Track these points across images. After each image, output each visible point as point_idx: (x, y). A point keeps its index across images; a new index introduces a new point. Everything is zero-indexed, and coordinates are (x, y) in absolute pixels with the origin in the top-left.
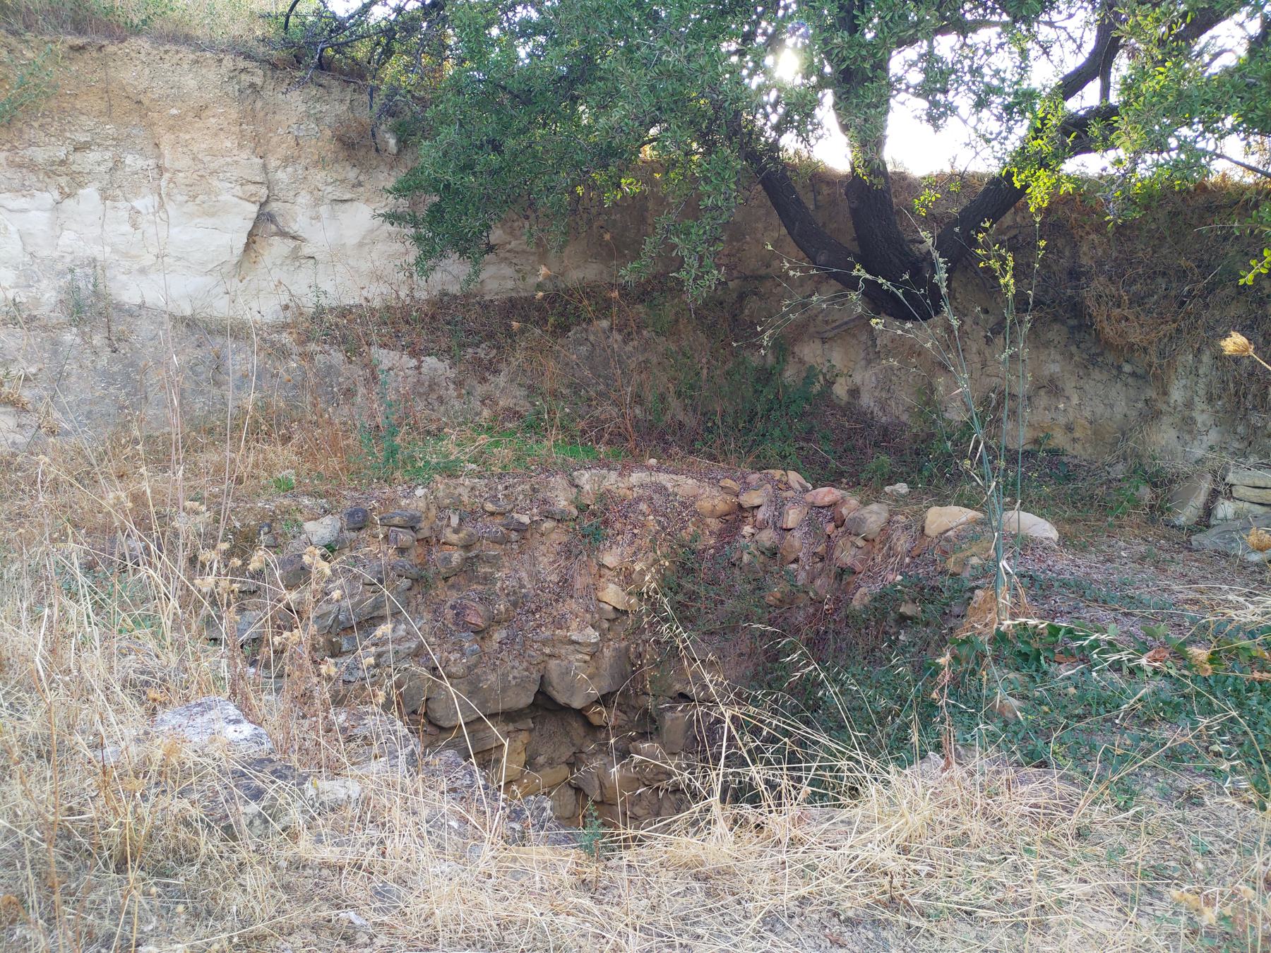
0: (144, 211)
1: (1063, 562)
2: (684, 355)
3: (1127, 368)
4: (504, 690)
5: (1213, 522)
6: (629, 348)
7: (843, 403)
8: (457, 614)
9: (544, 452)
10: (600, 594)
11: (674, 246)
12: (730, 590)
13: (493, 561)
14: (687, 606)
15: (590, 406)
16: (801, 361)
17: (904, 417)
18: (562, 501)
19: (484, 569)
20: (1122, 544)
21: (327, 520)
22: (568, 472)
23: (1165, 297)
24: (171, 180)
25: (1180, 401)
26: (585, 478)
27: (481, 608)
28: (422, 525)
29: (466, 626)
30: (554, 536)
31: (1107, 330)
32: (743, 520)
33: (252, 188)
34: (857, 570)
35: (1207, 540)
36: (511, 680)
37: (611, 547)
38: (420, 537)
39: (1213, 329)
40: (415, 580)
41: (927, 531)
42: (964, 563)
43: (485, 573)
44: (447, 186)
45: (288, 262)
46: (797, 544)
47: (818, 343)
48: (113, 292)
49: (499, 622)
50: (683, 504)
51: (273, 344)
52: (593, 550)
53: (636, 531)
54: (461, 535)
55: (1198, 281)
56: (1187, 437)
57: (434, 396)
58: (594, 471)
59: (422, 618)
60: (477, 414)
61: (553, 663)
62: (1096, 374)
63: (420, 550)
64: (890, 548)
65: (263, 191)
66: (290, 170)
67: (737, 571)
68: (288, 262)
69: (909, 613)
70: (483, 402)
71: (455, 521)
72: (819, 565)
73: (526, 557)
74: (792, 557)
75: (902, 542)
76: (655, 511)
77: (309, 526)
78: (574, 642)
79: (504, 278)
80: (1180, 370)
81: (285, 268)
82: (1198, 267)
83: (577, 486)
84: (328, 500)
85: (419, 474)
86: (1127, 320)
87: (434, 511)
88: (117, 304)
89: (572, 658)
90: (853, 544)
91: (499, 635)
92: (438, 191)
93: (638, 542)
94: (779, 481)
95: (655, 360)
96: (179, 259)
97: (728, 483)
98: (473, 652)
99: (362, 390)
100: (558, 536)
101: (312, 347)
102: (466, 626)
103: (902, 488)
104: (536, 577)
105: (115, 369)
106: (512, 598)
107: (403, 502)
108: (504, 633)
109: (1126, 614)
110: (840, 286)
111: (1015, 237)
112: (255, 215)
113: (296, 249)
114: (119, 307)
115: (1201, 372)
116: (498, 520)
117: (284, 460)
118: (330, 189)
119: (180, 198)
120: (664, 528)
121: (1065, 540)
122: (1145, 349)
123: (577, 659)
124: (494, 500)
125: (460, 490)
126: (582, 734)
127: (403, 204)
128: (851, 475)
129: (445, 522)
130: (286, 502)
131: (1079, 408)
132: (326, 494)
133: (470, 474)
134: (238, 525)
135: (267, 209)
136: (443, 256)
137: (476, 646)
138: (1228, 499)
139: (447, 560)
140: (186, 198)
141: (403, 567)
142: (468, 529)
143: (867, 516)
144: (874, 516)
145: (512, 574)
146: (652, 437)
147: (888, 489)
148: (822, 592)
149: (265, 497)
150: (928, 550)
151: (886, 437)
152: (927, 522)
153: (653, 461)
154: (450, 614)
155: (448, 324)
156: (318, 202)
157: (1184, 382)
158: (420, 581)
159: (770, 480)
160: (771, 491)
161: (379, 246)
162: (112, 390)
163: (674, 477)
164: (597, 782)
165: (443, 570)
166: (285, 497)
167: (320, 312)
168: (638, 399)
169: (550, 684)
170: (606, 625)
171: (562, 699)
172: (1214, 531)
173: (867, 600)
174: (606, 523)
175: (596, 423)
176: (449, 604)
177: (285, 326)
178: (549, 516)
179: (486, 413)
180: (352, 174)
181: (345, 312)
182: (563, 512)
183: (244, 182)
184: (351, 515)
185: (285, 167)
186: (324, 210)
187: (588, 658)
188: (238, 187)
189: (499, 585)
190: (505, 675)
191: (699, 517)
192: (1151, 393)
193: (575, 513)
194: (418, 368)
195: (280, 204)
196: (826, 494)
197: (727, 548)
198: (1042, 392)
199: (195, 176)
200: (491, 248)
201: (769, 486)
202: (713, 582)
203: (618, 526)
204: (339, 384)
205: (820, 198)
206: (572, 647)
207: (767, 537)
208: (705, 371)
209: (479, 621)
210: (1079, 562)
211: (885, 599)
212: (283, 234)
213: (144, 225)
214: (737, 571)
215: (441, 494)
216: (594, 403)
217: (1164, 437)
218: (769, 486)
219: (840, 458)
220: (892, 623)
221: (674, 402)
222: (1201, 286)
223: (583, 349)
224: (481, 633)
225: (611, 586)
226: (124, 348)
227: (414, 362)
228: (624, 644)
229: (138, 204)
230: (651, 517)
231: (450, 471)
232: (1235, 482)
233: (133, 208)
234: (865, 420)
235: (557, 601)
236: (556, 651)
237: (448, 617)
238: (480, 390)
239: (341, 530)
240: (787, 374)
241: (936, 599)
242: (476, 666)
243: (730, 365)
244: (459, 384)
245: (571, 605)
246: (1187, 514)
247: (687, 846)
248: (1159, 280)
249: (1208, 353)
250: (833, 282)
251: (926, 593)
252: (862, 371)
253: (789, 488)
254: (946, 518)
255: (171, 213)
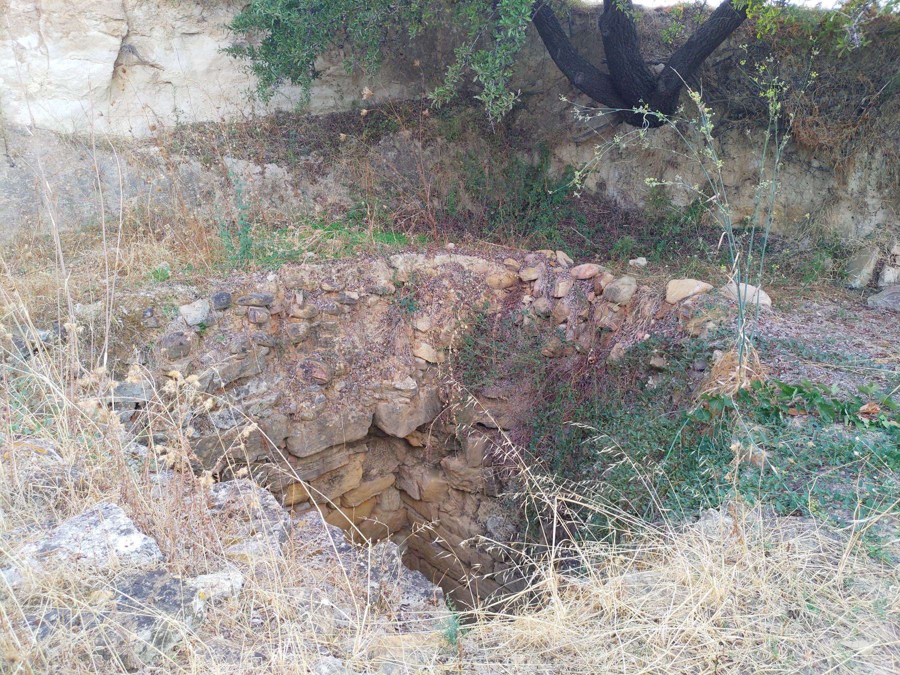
0: (27, 47)
1: (777, 323)
2: (471, 157)
3: (815, 164)
4: (346, 427)
5: (881, 284)
6: (427, 152)
7: (593, 194)
8: (306, 372)
9: (366, 240)
10: (415, 351)
11: (475, 73)
12: (514, 345)
13: (332, 329)
14: (482, 359)
15: (398, 200)
16: (560, 161)
17: (641, 204)
18: (383, 280)
19: (324, 336)
20: (816, 305)
21: (198, 303)
22: (385, 255)
23: (847, 106)
24: (47, 20)
25: (856, 189)
26: (399, 261)
27: (324, 367)
28: (274, 303)
29: (314, 381)
30: (378, 307)
31: (802, 133)
32: (522, 290)
33: (115, 24)
34: (613, 329)
35: (879, 300)
36: (350, 420)
37: (422, 315)
38: (273, 312)
39: (884, 132)
40: (272, 348)
41: (668, 299)
42: (702, 327)
43: (326, 338)
44: (277, 22)
45: (150, 86)
46: (566, 309)
47: (573, 146)
48: (7, 116)
49: (339, 376)
50: (476, 279)
51: (143, 156)
52: (408, 318)
53: (441, 302)
54: (305, 310)
55: (873, 93)
56: (860, 217)
57: (275, 196)
58: (406, 255)
59: (279, 376)
60: (311, 209)
61: (382, 405)
62: (791, 169)
63: (274, 323)
64: (638, 312)
65: (124, 27)
66: (145, 8)
67: (519, 330)
68: (150, 86)
69: (657, 365)
70: (315, 199)
71: (300, 299)
72: (583, 325)
73: (357, 324)
74: (562, 319)
75: (648, 308)
76: (455, 286)
77: (184, 309)
78: (397, 389)
79: (326, 97)
80: (857, 165)
81: (148, 92)
82: (873, 81)
83: (394, 268)
84: (197, 285)
85: (269, 263)
86: (817, 125)
87: (282, 291)
88: (12, 126)
89: (396, 401)
90: (610, 309)
91: (339, 385)
92: (269, 26)
93: (443, 310)
94: (550, 259)
95: (447, 161)
96: (59, 86)
97: (511, 262)
98: (320, 400)
99: (218, 194)
100: (381, 308)
101: (176, 158)
102: (314, 381)
103: (642, 261)
104: (365, 339)
105: (14, 181)
106: (348, 357)
107: (258, 286)
108: (343, 384)
109: (836, 370)
110: (590, 100)
111: (729, 58)
112: (118, 48)
113: (155, 75)
114: (13, 129)
115: (873, 166)
116: (334, 297)
117: (159, 254)
118: (179, 24)
119: (56, 35)
120: (462, 299)
121: (777, 305)
122: (832, 148)
123: (400, 402)
124: (330, 280)
125: (301, 274)
126: (404, 452)
127: (241, 38)
128: (603, 252)
129: (292, 300)
130: (164, 290)
131: (773, 192)
132: (197, 282)
133: (310, 261)
134: (125, 312)
135: (128, 42)
136: (279, 83)
137: (322, 396)
138: (893, 266)
139: (295, 330)
140: (60, 34)
141: (262, 338)
142: (310, 305)
143: (621, 287)
144: (626, 286)
145: (347, 338)
146: (452, 224)
147: (631, 262)
148: (585, 346)
149: (146, 287)
150: (669, 314)
151: (628, 220)
152: (668, 292)
153: (451, 245)
154: (300, 372)
155: (284, 136)
156: (170, 35)
157: (859, 174)
158: (276, 348)
159: (543, 258)
160: (544, 267)
161: (223, 72)
162: (13, 198)
163: (468, 257)
164: (416, 487)
165: (293, 338)
166: (162, 286)
167: (181, 128)
168: (435, 193)
169: (380, 420)
170: (421, 374)
171: (389, 431)
172: (884, 293)
173: (622, 353)
174: (418, 296)
175: (405, 215)
176: (299, 364)
177: (154, 142)
178: (374, 292)
179: (318, 208)
180: (197, 11)
181: (198, 127)
182: (384, 288)
183: (107, 20)
184: (217, 298)
185: (141, 6)
186: (176, 42)
187: (408, 400)
188: (103, 24)
189: (337, 347)
190: (346, 416)
191: (489, 289)
192: (833, 183)
193: (393, 289)
194: (262, 173)
195: (138, 37)
196: (587, 269)
197: (511, 313)
198: (748, 183)
199: (66, 16)
200: (316, 74)
201: (543, 264)
202: (500, 340)
203: (427, 298)
204: (200, 188)
205: (574, 27)
206: (396, 393)
207: (542, 304)
208: (487, 169)
209: (323, 376)
210: (789, 323)
211: (637, 352)
212: (143, 63)
213: (29, 59)
214: (519, 330)
215: (287, 278)
216: (401, 197)
217: (841, 218)
218: (543, 264)
219: (593, 237)
220: (642, 372)
221: (465, 197)
222: (874, 97)
223: (392, 154)
224: (326, 385)
225: (424, 345)
226: (20, 163)
227: (258, 169)
228: (435, 387)
229: (23, 41)
230: (452, 291)
231: (293, 259)
232: (898, 253)
233: (18, 44)
234: (610, 207)
235: (383, 358)
236: (384, 396)
237: (299, 374)
238: (312, 189)
239: (210, 311)
240: (550, 171)
241: (682, 355)
242: (323, 410)
243: (506, 164)
244: (296, 186)
245: (394, 360)
246: (861, 279)
247: (530, 625)
248: (842, 92)
249: (880, 151)
250: (585, 96)
251: (673, 351)
252: (597, 163)
253: (558, 265)
254: (683, 288)
255: (50, 47)
